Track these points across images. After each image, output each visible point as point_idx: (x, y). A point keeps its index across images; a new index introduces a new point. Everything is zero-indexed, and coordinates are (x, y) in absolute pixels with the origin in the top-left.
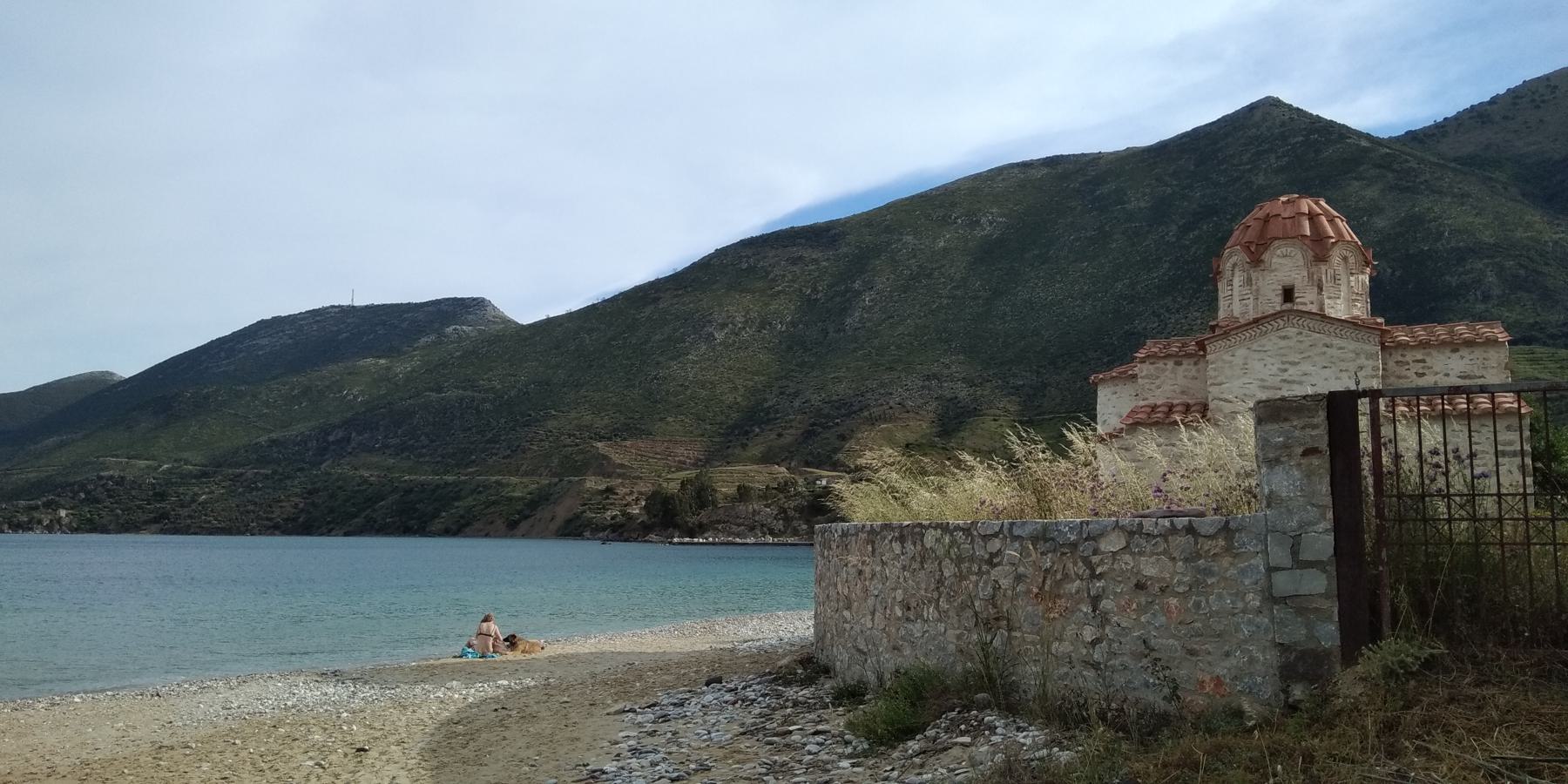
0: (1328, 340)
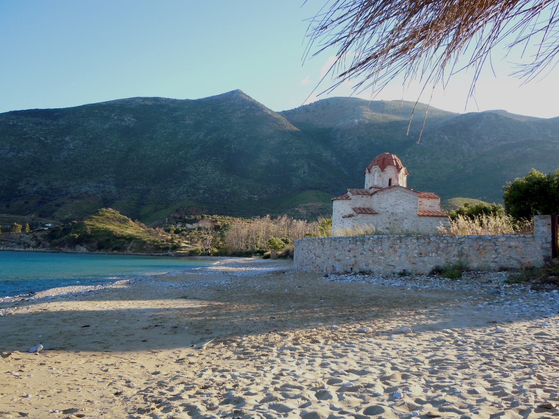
0: (407, 194)
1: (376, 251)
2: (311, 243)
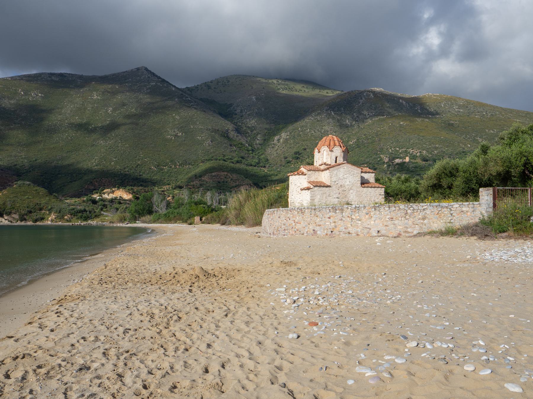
1: (354, 217)
2: (290, 212)
